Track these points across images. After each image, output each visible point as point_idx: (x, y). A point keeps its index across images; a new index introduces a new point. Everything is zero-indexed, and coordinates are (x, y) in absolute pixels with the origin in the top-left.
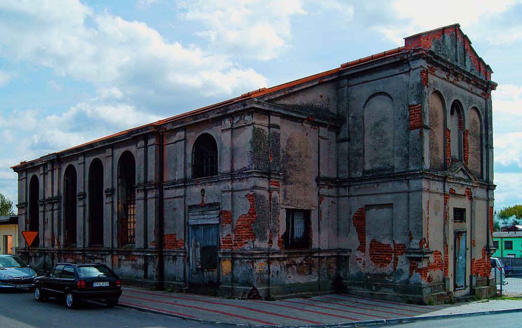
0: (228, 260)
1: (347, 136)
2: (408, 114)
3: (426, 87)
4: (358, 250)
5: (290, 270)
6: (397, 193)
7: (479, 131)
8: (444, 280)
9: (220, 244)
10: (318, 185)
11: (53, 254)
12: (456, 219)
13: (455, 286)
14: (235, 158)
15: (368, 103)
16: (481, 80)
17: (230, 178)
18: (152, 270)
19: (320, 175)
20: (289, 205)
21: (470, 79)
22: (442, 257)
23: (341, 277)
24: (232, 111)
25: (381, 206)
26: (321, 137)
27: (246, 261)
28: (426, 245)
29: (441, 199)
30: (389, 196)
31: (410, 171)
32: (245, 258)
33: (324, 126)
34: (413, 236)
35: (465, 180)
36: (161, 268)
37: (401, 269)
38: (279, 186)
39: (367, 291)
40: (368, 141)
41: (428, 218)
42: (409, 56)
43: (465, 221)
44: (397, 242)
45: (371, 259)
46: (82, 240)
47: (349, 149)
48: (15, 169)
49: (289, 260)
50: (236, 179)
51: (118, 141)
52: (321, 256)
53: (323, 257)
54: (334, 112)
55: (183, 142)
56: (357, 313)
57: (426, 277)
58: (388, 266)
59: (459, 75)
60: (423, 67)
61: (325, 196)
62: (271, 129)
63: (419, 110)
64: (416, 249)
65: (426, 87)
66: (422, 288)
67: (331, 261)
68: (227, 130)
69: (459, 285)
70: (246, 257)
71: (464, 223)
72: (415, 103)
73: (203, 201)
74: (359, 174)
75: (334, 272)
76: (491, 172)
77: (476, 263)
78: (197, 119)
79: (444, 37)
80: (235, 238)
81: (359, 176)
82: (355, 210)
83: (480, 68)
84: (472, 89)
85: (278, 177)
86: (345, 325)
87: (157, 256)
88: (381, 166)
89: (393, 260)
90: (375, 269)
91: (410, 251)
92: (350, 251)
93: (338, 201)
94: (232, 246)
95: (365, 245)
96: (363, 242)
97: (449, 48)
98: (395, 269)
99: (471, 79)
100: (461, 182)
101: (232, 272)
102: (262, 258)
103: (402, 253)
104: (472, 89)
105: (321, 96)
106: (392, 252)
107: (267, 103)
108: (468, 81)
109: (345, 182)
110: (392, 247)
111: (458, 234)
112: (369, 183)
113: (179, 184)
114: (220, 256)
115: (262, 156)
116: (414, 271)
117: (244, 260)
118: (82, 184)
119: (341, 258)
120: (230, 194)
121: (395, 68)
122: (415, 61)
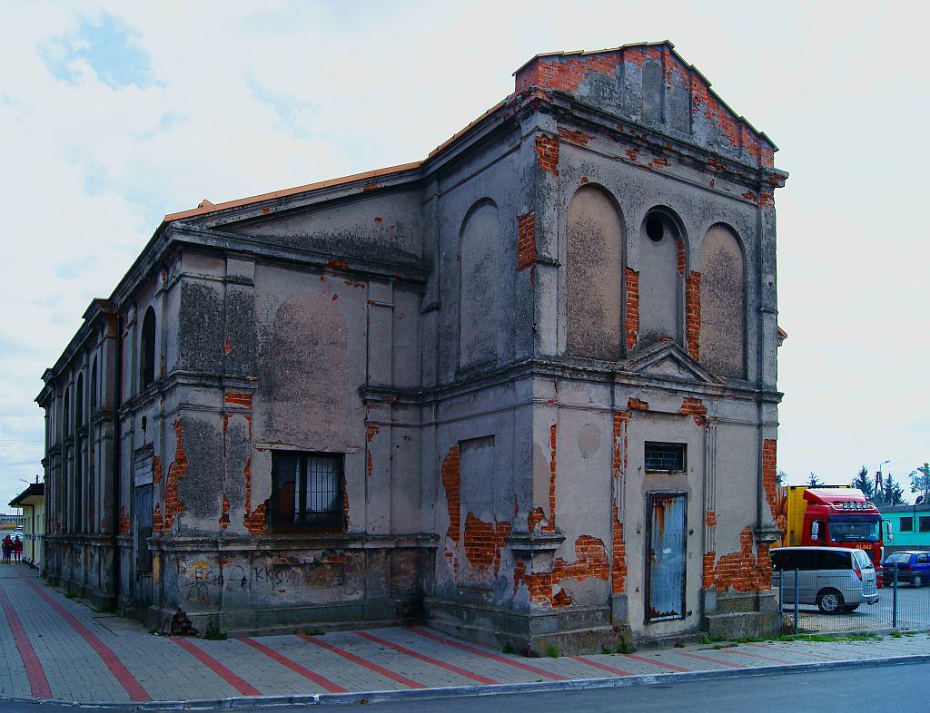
3: (549, 175)
4: (448, 535)
5: (284, 575)
8: (610, 601)
10: (365, 402)
13: (650, 614)
19: (370, 381)
20: (279, 442)
21: (726, 170)
22: (608, 548)
29: (606, 423)
30: (490, 420)
33: (384, 279)
35: (678, 382)
39: (816, 608)
43: (685, 471)
45: (468, 555)
49: (279, 557)
53: (376, 551)
60: (539, 130)
61: (381, 424)
62: (229, 286)
65: (549, 175)
66: (527, 620)
67: (401, 559)
74: (450, 377)
75: (411, 582)
79: (622, 70)
83: (741, 141)
85: (242, 385)
86: (195, 704)
87: (108, 548)
92: (437, 537)
94: (162, 527)
99: (706, 160)
100: (667, 386)
102: (200, 552)
104: (712, 184)
105: (378, 219)
108: (699, 166)
111: (657, 502)
116: (520, 580)
119: (422, 553)
121: (503, 143)
122: (529, 119)
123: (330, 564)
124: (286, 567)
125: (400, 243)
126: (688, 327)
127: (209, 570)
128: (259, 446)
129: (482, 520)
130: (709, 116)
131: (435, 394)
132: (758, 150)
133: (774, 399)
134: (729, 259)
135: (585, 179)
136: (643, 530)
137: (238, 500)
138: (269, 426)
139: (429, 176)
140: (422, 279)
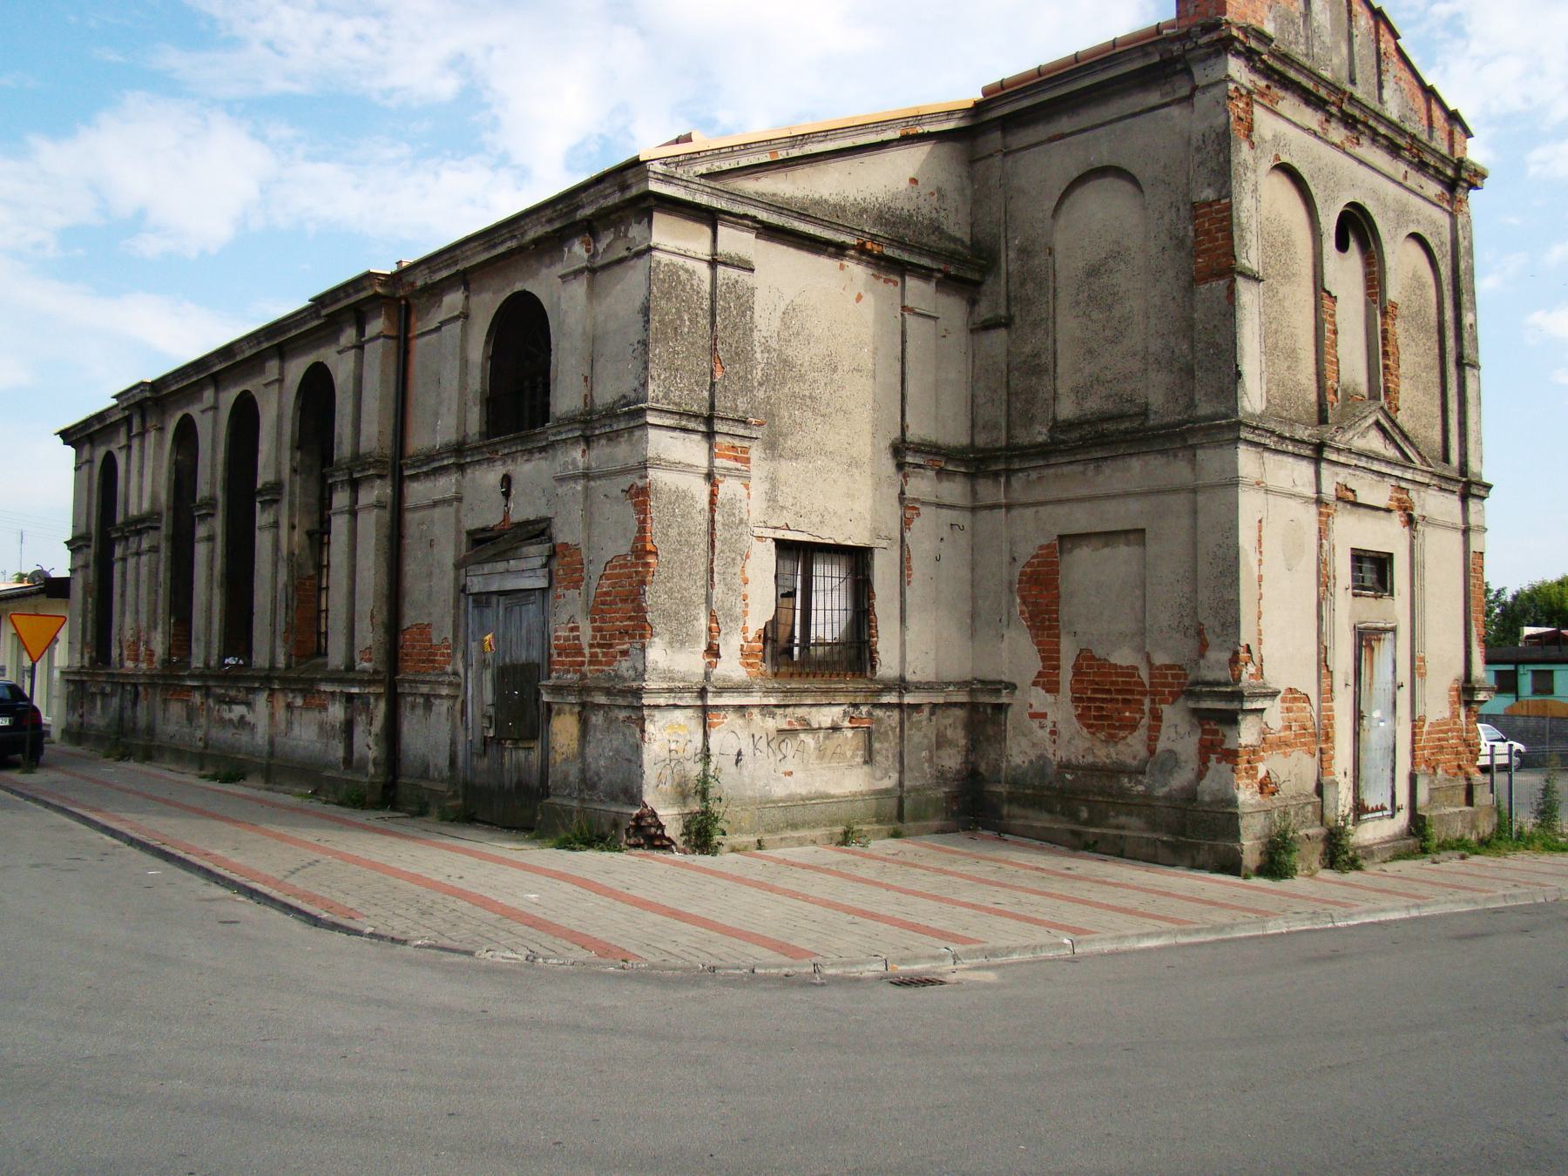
0: (572, 713)
1: (1002, 312)
2: (1192, 234)
3: (1245, 146)
4: (1035, 684)
5: (790, 747)
6: (1160, 492)
7: (1433, 311)
8: (1319, 790)
9: (550, 656)
10: (900, 466)
11: (135, 686)
12: (1359, 587)
14: (598, 367)
15: (1067, 203)
16: (1434, 151)
17: (578, 433)
18: (367, 744)
22: (1312, 710)
23: (981, 774)
24: (588, 211)
25: (1108, 537)
26: (911, 311)
27: (622, 715)
28: (1251, 669)
30: (1134, 506)
31: (1197, 420)
32: (619, 707)
33: (924, 274)
34: (1209, 637)
35: (1388, 462)
36: (392, 734)
37: (1170, 751)
38: (748, 461)
40: (1068, 325)
41: (1260, 578)
42: (1189, 46)
43: (1392, 594)
44: (1160, 659)
45: (1079, 717)
46: (205, 649)
47: (1009, 352)
48: (67, 436)
50: (599, 436)
51: (293, 333)
52: (909, 705)
53: (917, 707)
54: (958, 235)
55: (459, 323)
56: (1050, 895)
57: (1254, 776)
58: (1129, 740)
59: (1359, 126)
61: (923, 503)
62: (720, 269)
63: (1222, 220)
64: (1218, 684)
66: (1234, 818)
68: (577, 273)
69: (1371, 800)
70: (620, 701)
71: (1386, 601)
72: (1208, 194)
73: (506, 514)
74: (1040, 434)
76: (1476, 442)
77: (1429, 733)
78: (494, 246)
80: (594, 637)
81: (1040, 439)
82: (1026, 551)
84: (1405, 178)
87: (378, 696)
88: (1109, 407)
89: (1145, 721)
90: (1090, 750)
91: (1198, 688)
92: (1012, 687)
93: (973, 524)
94: (583, 663)
95: (1058, 667)
96: (1052, 659)
97: (1327, 40)
98: (1152, 751)
100: (1376, 466)
101: (582, 754)
103: (1175, 696)
104: (1405, 178)
106: (1144, 694)
107: (703, 181)
108: (1394, 150)
109: (996, 459)
110: (1144, 674)
111: (1366, 638)
112: (1071, 463)
113: (443, 459)
114: (546, 698)
115: (686, 358)
116: (1213, 757)
117: (616, 711)
118: (210, 477)
120: (579, 488)
123: (852, 728)
124: (792, 732)
125: (942, 219)
126: (1386, 381)
127: (688, 738)
128: (758, 532)
129: (1112, 660)
130: (1397, 80)
131: (1008, 459)
132: (1451, 134)
133: (1482, 493)
134: (1422, 286)
135: (1277, 157)
136: (1351, 682)
137: (731, 620)
138: (772, 499)
139: (984, 123)
140: (977, 277)
